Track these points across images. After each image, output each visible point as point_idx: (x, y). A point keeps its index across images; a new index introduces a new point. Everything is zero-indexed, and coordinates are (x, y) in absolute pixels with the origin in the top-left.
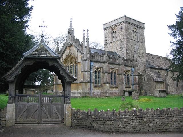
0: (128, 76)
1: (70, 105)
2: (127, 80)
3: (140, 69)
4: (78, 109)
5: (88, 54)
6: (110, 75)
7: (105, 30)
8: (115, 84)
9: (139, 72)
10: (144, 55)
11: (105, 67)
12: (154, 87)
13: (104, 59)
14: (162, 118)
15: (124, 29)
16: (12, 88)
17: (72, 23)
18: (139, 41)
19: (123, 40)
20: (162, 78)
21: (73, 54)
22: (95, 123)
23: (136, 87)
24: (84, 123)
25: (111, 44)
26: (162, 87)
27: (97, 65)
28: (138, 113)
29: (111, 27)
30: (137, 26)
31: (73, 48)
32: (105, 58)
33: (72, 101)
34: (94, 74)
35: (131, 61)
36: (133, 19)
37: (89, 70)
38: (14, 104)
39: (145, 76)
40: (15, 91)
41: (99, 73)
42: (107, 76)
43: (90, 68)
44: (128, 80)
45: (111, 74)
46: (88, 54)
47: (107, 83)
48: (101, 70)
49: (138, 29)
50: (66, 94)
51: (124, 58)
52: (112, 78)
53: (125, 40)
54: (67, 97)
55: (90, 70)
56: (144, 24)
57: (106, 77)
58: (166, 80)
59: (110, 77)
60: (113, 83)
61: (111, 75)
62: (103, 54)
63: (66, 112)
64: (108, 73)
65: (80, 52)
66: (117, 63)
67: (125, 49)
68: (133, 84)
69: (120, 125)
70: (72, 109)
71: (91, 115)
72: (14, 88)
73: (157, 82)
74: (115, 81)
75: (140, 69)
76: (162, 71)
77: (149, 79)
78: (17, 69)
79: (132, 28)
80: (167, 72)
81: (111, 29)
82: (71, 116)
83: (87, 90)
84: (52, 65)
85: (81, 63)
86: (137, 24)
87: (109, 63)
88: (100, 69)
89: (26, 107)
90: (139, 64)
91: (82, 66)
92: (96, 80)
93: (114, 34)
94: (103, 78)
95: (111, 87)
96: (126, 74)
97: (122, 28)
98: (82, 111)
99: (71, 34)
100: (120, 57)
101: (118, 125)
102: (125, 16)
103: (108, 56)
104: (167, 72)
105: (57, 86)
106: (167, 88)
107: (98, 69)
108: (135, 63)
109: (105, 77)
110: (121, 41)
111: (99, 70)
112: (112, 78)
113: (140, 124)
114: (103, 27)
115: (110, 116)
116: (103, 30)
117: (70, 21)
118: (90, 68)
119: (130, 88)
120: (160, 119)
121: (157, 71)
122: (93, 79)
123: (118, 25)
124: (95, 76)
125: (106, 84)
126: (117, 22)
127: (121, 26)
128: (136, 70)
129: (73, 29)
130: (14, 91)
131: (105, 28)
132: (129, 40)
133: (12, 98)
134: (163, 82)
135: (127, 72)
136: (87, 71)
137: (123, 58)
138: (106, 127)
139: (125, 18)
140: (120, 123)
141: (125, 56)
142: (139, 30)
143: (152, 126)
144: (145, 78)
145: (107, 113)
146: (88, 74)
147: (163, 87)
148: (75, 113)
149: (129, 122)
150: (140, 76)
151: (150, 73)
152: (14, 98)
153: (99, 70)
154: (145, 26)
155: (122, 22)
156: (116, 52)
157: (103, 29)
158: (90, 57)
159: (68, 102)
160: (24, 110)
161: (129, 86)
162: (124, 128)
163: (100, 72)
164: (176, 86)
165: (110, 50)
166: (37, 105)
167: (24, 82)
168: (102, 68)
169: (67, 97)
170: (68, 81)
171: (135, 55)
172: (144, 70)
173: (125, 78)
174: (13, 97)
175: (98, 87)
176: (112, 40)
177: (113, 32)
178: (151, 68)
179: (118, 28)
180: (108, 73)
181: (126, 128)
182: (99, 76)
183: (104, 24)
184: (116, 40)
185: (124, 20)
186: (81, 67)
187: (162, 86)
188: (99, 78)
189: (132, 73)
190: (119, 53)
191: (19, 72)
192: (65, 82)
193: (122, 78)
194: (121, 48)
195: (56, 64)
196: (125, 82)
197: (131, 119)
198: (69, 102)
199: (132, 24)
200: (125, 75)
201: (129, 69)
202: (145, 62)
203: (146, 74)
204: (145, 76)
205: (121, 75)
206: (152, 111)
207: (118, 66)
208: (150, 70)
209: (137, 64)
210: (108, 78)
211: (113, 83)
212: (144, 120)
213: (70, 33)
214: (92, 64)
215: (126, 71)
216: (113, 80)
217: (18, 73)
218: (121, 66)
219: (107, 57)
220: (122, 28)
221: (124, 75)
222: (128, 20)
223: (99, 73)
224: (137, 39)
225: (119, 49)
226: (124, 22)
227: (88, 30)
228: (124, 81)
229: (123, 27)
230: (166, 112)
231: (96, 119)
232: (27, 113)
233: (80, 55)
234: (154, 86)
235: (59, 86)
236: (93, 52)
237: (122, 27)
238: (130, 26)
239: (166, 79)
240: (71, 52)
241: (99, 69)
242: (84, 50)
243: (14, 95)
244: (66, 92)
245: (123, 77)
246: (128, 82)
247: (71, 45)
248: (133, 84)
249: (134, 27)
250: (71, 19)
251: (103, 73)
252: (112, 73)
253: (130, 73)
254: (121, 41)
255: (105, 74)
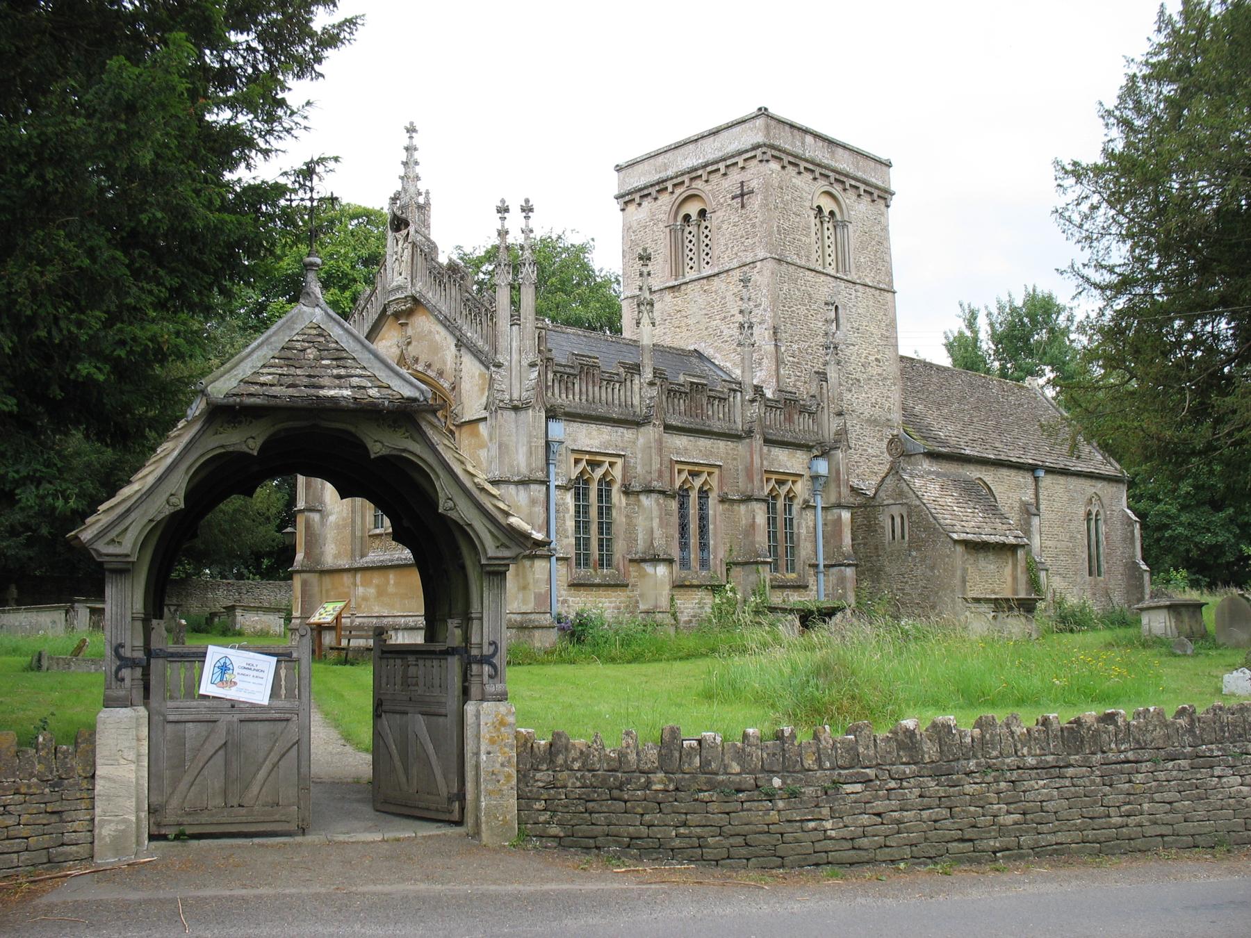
0: (788, 508)
1: (502, 708)
2: (781, 536)
3: (866, 464)
4: (557, 735)
5: (533, 365)
6: (674, 505)
7: (631, 208)
8: (704, 564)
9: (855, 482)
10: (893, 369)
11: (639, 450)
12: (957, 581)
13: (636, 401)
14: (1070, 771)
15: (755, 202)
16: (124, 600)
17: (417, 155)
18: (853, 276)
19: (755, 277)
20: (1003, 517)
21: (429, 366)
22: (668, 819)
23: (842, 580)
24: (600, 818)
25: (668, 297)
26: (1000, 579)
27: (591, 438)
28: (930, 750)
29: (669, 185)
30: (841, 178)
31: (423, 323)
32: (640, 394)
33: (516, 679)
34: (569, 498)
35: (804, 410)
36: (816, 136)
37: (540, 475)
38: (142, 711)
39: (896, 511)
40: (146, 621)
41: (605, 494)
42: (655, 513)
43: (548, 464)
44: (790, 537)
45: (685, 497)
46: (533, 365)
47: (655, 560)
48: (617, 472)
49: (848, 199)
50: (475, 639)
51: (763, 395)
52: (683, 528)
53: (767, 273)
54: (484, 660)
55: (548, 476)
56: (888, 165)
57: (647, 521)
58: (1027, 532)
59: (675, 519)
60: (694, 555)
61: (683, 506)
62: (623, 365)
63: (484, 757)
64: (663, 493)
65: (476, 353)
66: (717, 426)
67: (768, 334)
68: (821, 563)
69: (828, 825)
70: (517, 735)
71: (642, 766)
72: (139, 606)
73: (977, 547)
74: (704, 546)
75: (866, 464)
76: (1004, 472)
77: (923, 528)
78: (158, 479)
79: (811, 191)
80: (1036, 479)
81: (677, 194)
82: (514, 782)
83: (529, 607)
84: (384, 452)
85: (483, 428)
86: (843, 163)
87: (668, 428)
88: (611, 464)
89: (221, 728)
90: (855, 427)
91: (494, 450)
92: (582, 543)
93: (693, 229)
94: (631, 528)
95: (679, 586)
96: (774, 498)
97: (743, 194)
98: (579, 742)
99: (412, 229)
100: (737, 387)
101: (812, 825)
102: (763, 112)
103: (658, 381)
104: (1036, 479)
105: (313, 578)
106: (1034, 584)
107: (594, 464)
108: (831, 426)
109: (641, 523)
110: (745, 281)
111: (599, 473)
112: (683, 528)
113: (945, 812)
114: (612, 184)
115: (763, 770)
116: (616, 206)
117: (406, 142)
118: (548, 464)
119: (801, 587)
120: (1059, 783)
121: (973, 473)
122: (561, 532)
123: (718, 175)
124: (577, 512)
125: (649, 568)
126: (711, 150)
127: (735, 176)
128: (838, 472)
129: (421, 200)
130: (139, 625)
131: (628, 188)
132: (792, 268)
133: (126, 673)
134: (1013, 548)
135: (781, 483)
136: (524, 482)
137: (758, 389)
138: (740, 840)
139: (767, 127)
140: (826, 811)
141: (763, 376)
142: (857, 209)
143: (1015, 823)
144: (898, 520)
145: (740, 755)
146: (533, 502)
147: (1015, 578)
148: (539, 759)
149: (879, 805)
150: (865, 508)
151: (931, 488)
152: (138, 672)
153: (599, 473)
154: (896, 179)
155: (747, 151)
156: (709, 352)
157: (617, 198)
158: (542, 387)
159: (491, 688)
160: (209, 749)
161: (794, 575)
162: (848, 845)
163: (605, 482)
164: (1090, 574)
165: (668, 341)
166: (291, 711)
167: (169, 569)
168: (620, 462)
169: (484, 660)
170: (490, 555)
171: (832, 373)
172: (894, 470)
173: (771, 521)
174: (132, 663)
175: (599, 586)
176: (677, 271)
177: (687, 218)
178: (933, 456)
179: (718, 190)
180: (663, 493)
181: (858, 843)
182: (600, 514)
183: (622, 161)
184: (707, 271)
185: (760, 138)
186: (483, 454)
187: (1008, 570)
188: (605, 527)
189: (814, 493)
190: (728, 361)
191: (173, 500)
192: (469, 564)
193: (753, 525)
194: (742, 326)
195: (416, 448)
196: (773, 550)
197: (892, 784)
198: (499, 687)
199: (813, 163)
200: (770, 501)
201: (790, 461)
202: (897, 417)
203: (901, 494)
204: (896, 511)
205: (743, 508)
206: (1012, 733)
207: (721, 445)
208: (930, 473)
209: (842, 433)
210: (662, 524)
211: (694, 555)
212: (968, 789)
213: (407, 225)
214: (558, 429)
215: (774, 477)
216: (694, 541)
217: (168, 511)
218: (741, 448)
219: (651, 384)
220: (743, 194)
221: (763, 506)
222: (785, 141)
223: (600, 490)
224: (842, 263)
225: (731, 331)
226: (759, 152)
227: (527, 209)
228: (761, 539)
229: (754, 184)
230: (1096, 735)
231: (677, 789)
232: (227, 763)
233: (471, 368)
234: (959, 573)
235: (327, 580)
236: (560, 357)
237: (742, 183)
238: (797, 181)
239: (1029, 524)
240: (412, 351)
241: (599, 464)
242: (502, 343)
243: (140, 655)
244: (475, 625)
245: (760, 515)
246: (792, 550)
247: (416, 303)
248: (821, 563)
249: (822, 185)
250: (411, 130)
251: (627, 492)
252: (683, 494)
253: (801, 488)
254: (745, 281)
255: (643, 498)
